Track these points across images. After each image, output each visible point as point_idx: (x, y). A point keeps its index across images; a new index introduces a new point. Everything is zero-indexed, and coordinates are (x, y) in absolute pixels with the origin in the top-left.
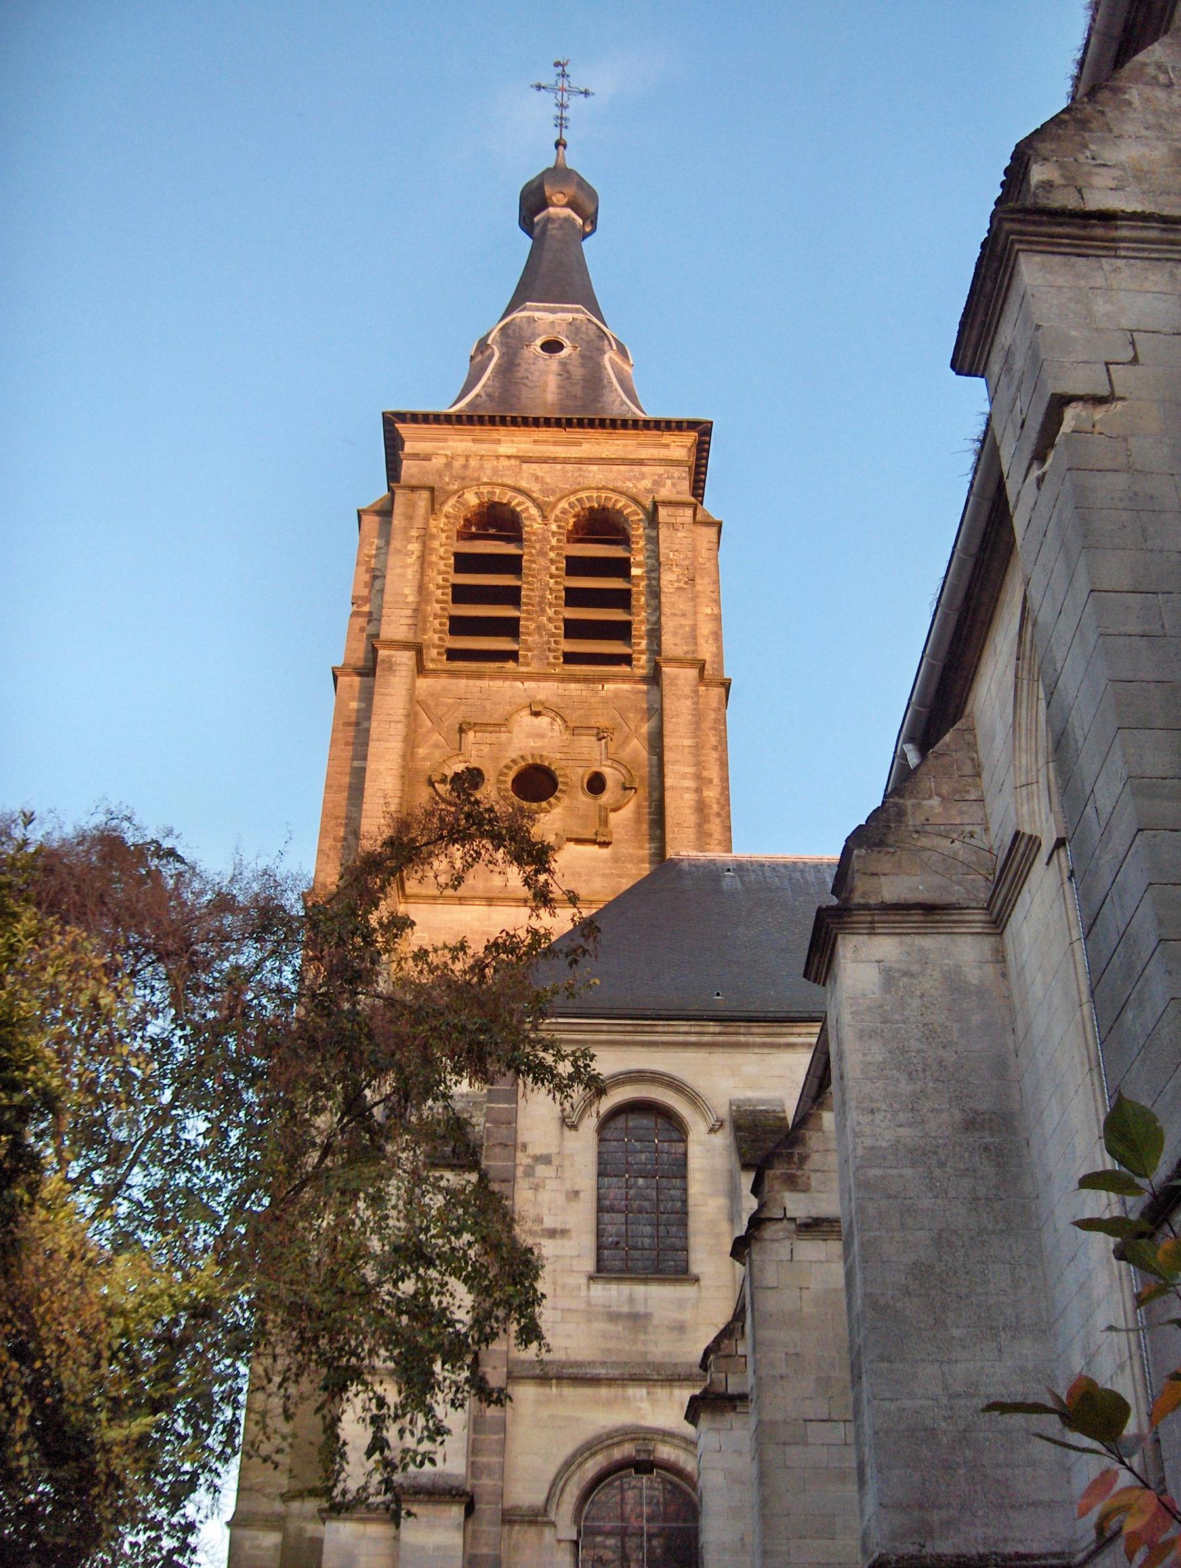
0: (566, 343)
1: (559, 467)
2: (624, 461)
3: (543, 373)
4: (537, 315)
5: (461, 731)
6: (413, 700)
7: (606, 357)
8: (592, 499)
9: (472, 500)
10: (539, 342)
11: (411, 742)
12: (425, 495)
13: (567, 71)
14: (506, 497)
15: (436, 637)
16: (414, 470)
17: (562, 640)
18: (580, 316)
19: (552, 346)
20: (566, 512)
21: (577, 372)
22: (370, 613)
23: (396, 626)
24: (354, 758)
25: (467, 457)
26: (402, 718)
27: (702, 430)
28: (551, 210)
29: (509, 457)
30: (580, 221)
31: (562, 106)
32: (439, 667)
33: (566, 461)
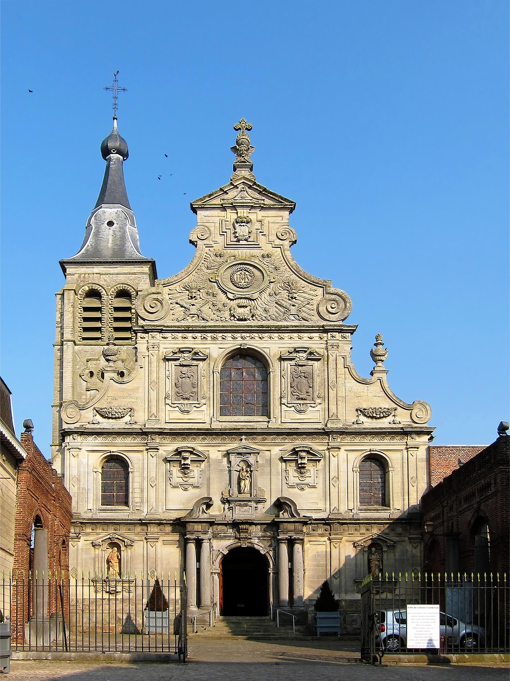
0: (115, 222)
1: (111, 276)
2: (130, 274)
3: (108, 235)
4: (106, 210)
5: (87, 361)
6: (74, 353)
7: (127, 227)
8: (121, 287)
9: (87, 288)
10: (106, 222)
11: (74, 366)
12: (73, 292)
13: (117, 79)
14: (96, 287)
15: (79, 334)
16: (70, 279)
17: (113, 312)
18: (120, 209)
19: (110, 224)
20: (113, 291)
21: (118, 234)
22: (61, 327)
23: (67, 336)
24: (60, 369)
25: (85, 274)
26: (71, 436)
27: (153, 264)
28: (111, 155)
29: (97, 274)
30: (122, 158)
31: (115, 98)
32: (81, 343)
33: (113, 274)
